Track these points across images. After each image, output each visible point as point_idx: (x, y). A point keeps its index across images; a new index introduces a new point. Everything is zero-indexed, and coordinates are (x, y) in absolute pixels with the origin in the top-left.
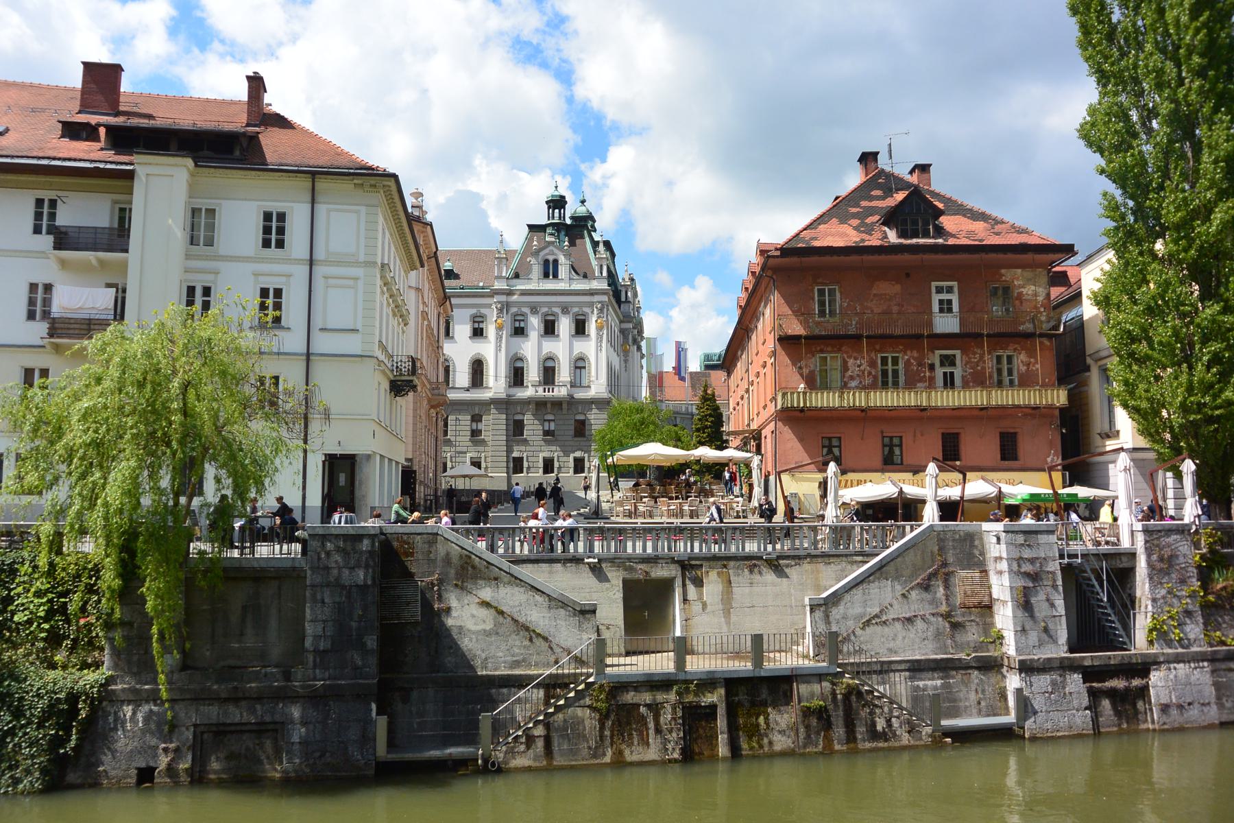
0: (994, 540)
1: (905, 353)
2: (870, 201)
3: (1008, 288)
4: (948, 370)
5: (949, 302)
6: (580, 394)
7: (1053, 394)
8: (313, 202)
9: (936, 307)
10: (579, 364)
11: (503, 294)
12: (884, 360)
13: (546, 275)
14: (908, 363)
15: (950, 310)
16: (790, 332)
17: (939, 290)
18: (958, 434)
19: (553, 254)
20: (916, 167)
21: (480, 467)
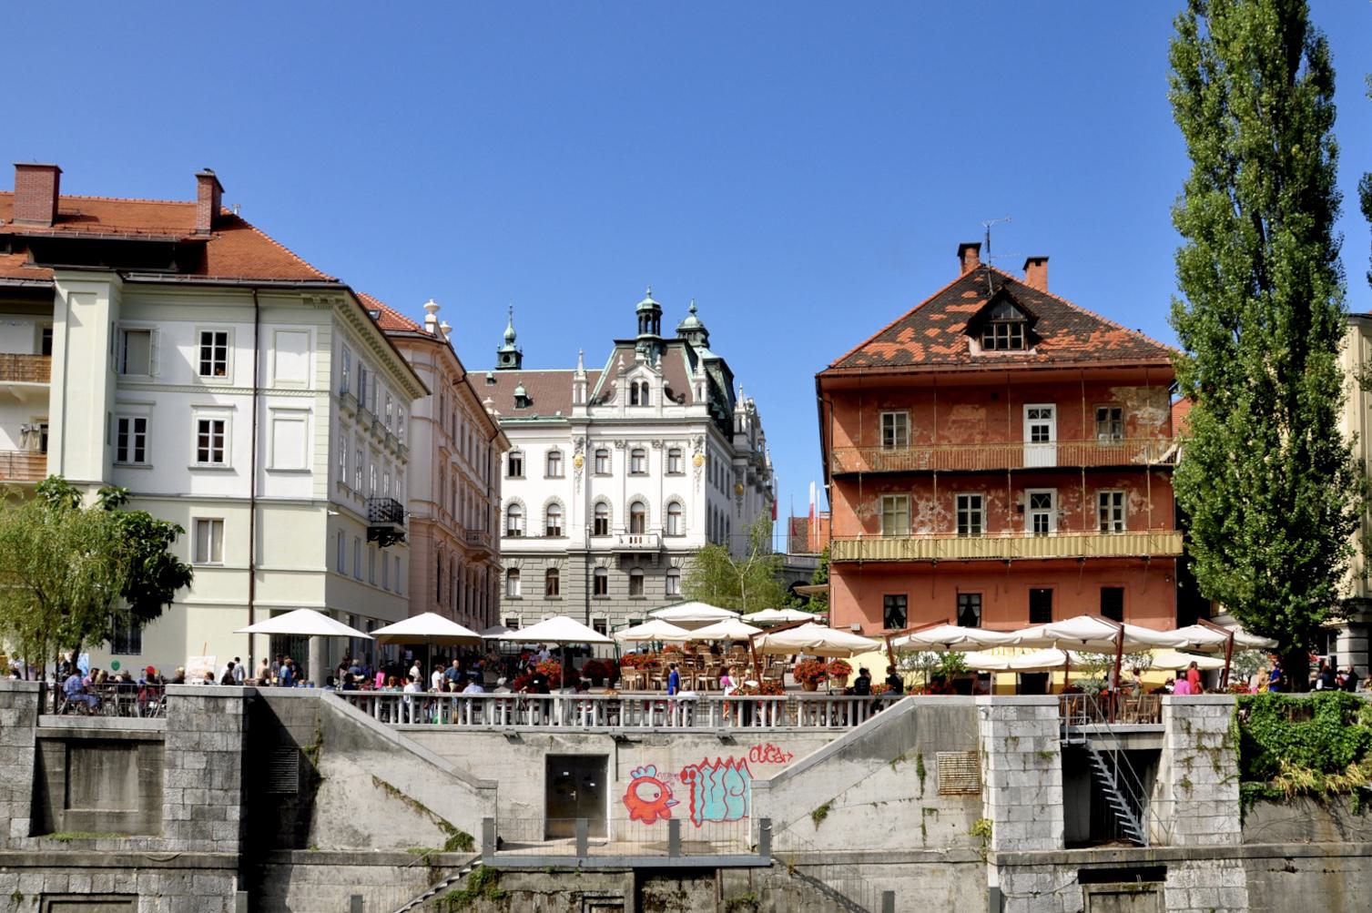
0: (983, 715)
1: (988, 493)
2: (959, 305)
3: (1119, 411)
4: (1041, 512)
5: (1045, 429)
6: (670, 543)
7: (1164, 541)
8: (257, 321)
9: (1028, 435)
10: (673, 508)
11: (582, 425)
12: (963, 503)
13: (634, 402)
14: (991, 505)
15: (1046, 439)
16: (849, 469)
17: (1033, 415)
18: (1121, 591)
19: (642, 377)
20: (1030, 261)
21: (604, 633)
